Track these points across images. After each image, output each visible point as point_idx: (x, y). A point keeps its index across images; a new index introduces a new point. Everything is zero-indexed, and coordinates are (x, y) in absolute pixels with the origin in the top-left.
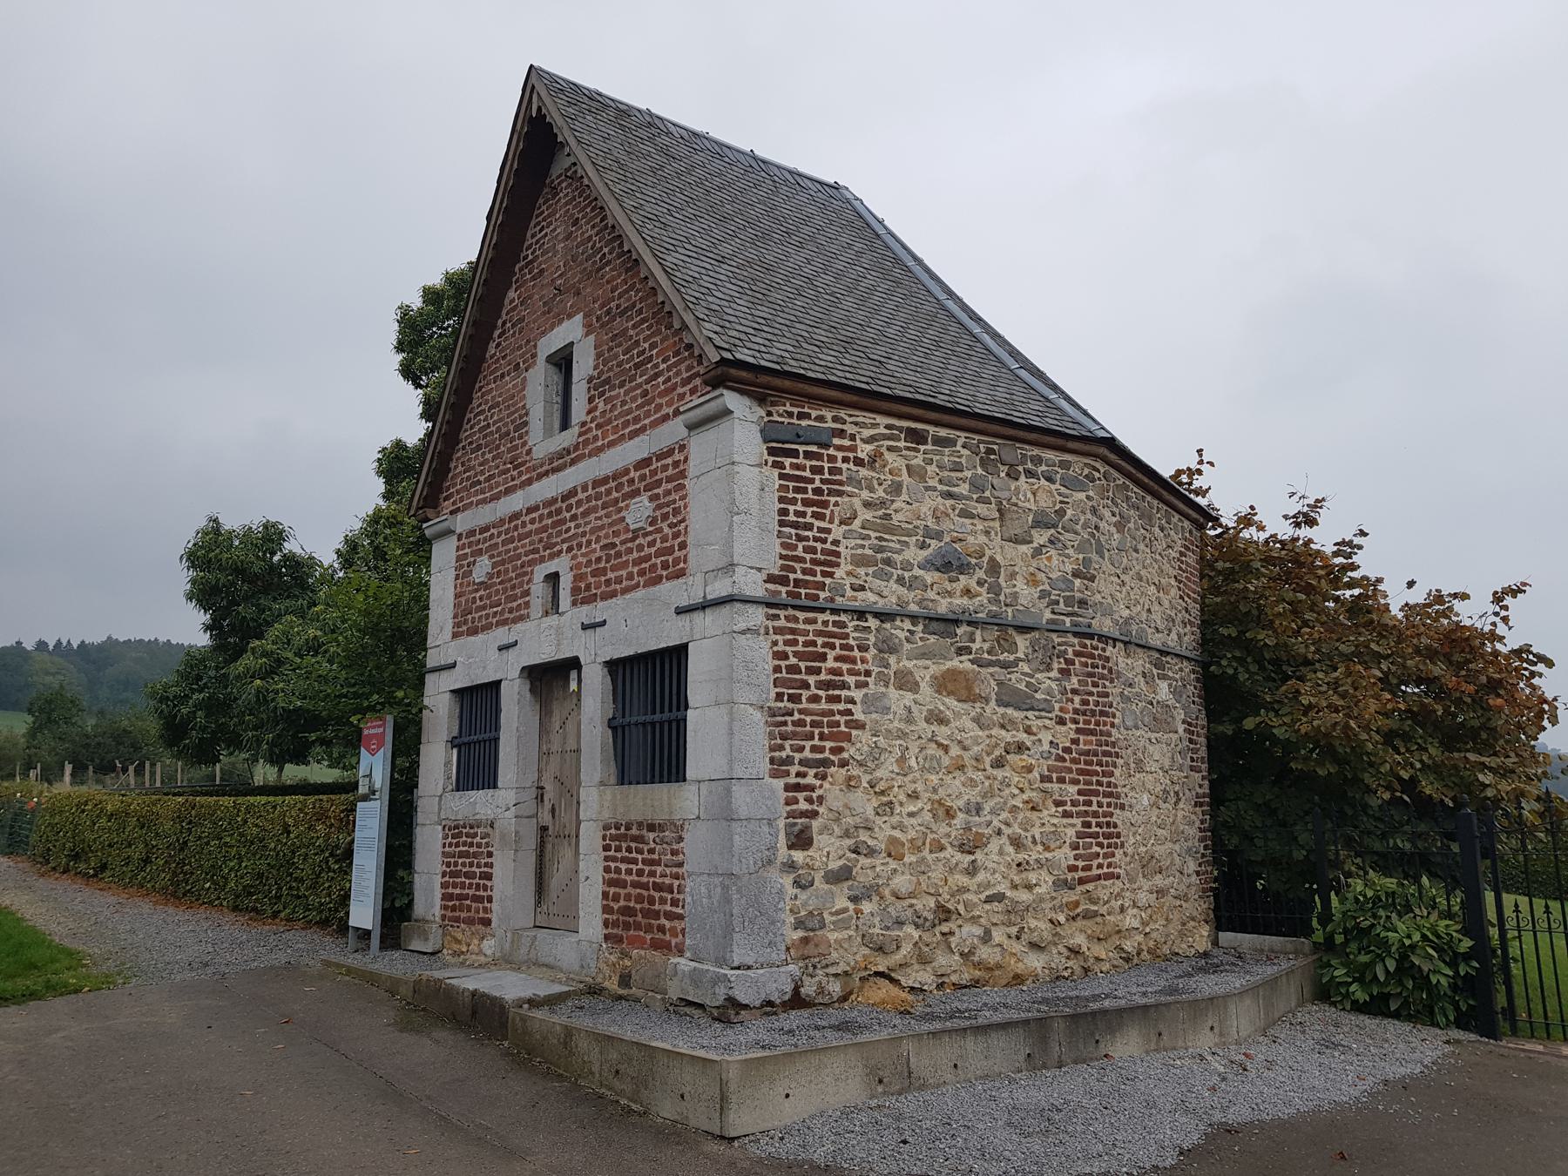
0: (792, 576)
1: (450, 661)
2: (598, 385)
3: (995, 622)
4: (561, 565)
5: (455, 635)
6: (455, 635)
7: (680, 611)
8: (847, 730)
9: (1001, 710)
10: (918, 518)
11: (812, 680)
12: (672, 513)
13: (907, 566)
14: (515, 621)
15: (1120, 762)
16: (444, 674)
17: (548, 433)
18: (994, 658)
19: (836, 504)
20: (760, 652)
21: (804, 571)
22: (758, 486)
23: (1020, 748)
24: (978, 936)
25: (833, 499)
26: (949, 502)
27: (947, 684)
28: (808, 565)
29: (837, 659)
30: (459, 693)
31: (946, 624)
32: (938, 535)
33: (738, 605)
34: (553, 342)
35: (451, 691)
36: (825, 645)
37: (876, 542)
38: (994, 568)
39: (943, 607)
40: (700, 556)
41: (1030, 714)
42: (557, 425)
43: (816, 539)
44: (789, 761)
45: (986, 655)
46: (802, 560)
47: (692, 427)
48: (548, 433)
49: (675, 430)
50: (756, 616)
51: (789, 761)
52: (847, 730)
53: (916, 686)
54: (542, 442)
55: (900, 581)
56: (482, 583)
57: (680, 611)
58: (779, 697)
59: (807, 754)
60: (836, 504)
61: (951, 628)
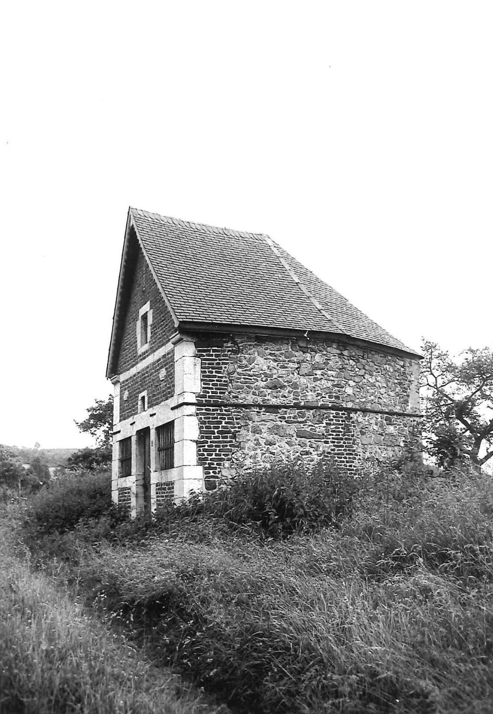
0: (208, 395)
1: (119, 430)
2: (154, 326)
3: (297, 406)
4: (144, 393)
5: (120, 421)
6: (120, 421)
7: (173, 409)
8: (230, 448)
9: (299, 439)
10: (262, 370)
11: (216, 431)
12: (170, 376)
13: (257, 388)
14: (134, 414)
15: (357, 457)
16: (118, 434)
17: (142, 345)
18: (296, 420)
19: (225, 367)
20: (194, 421)
21: (212, 393)
22: (194, 364)
23: (307, 453)
24: (49, 467)
25: (223, 366)
26: (276, 364)
27: (275, 430)
28: (214, 390)
29: (226, 423)
30: (121, 442)
31: (274, 409)
32: (271, 376)
33: (185, 406)
34: (142, 312)
35: (119, 441)
36: (221, 418)
37: (243, 380)
38: (295, 386)
39: (274, 401)
40: (178, 390)
41: (313, 440)
42: (144, 342)
43: (217, 381)
44: (206, 459)
45: (292, 419)
46: (212, 388)
47: (175, 344)
48: (142, 345)
49: (169, 346)
50: (192, 409)
51: (206, 459)
52: (230, 448)
53: (260, 432)
54: (141, 349)
55: (254, 394)
56: (126, 400)
57: (173, 409)
58: (202, 437)
59: (214, 456)
60: (225, 367)
61: (276, 410)
